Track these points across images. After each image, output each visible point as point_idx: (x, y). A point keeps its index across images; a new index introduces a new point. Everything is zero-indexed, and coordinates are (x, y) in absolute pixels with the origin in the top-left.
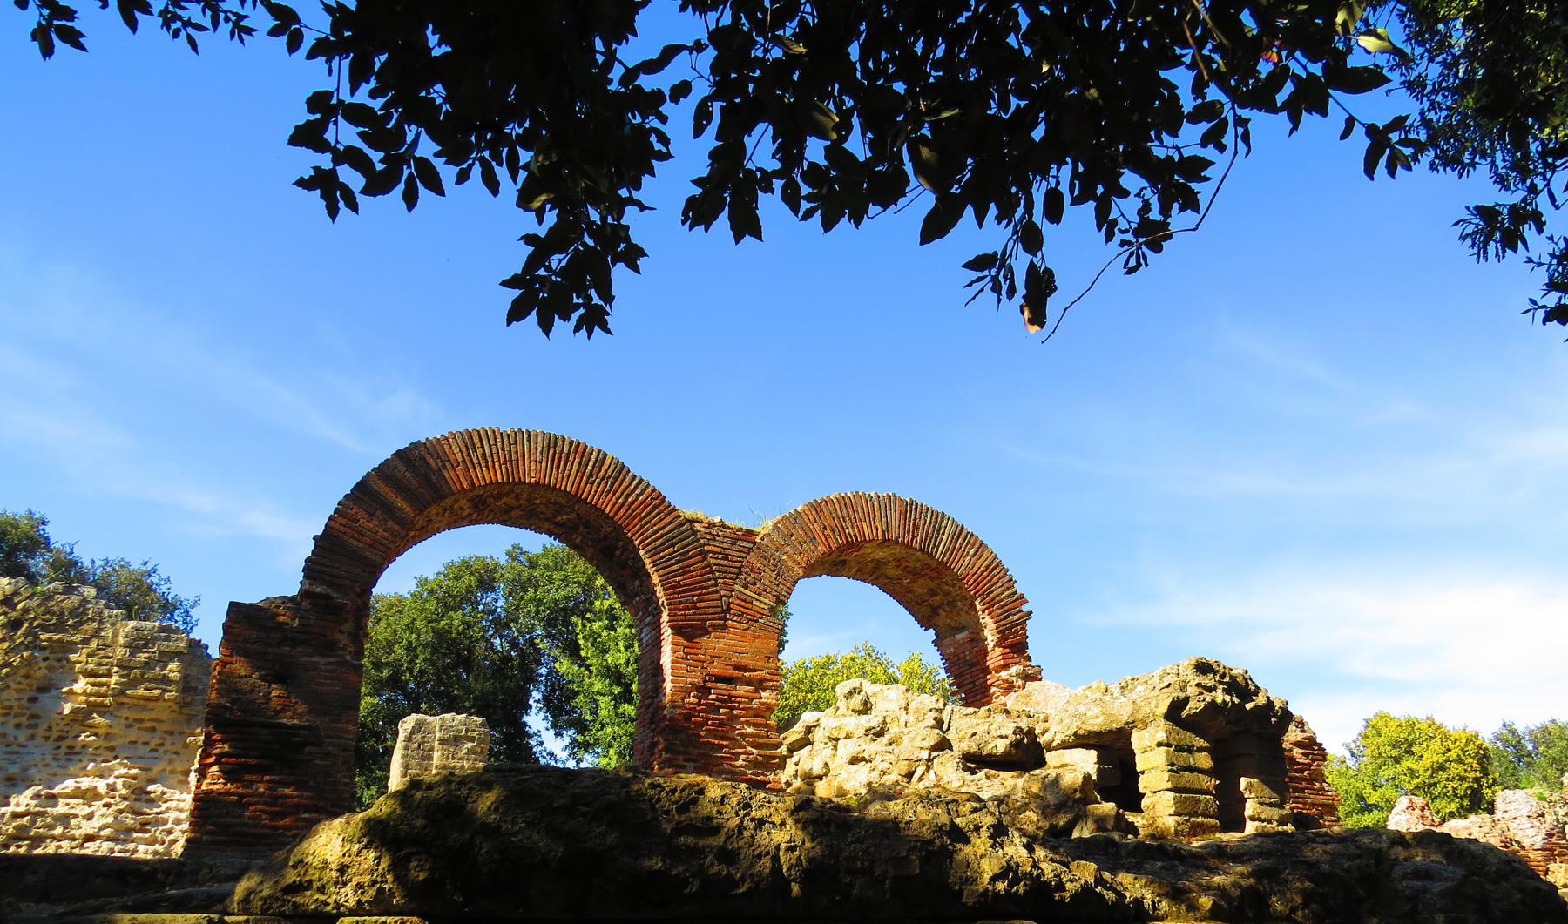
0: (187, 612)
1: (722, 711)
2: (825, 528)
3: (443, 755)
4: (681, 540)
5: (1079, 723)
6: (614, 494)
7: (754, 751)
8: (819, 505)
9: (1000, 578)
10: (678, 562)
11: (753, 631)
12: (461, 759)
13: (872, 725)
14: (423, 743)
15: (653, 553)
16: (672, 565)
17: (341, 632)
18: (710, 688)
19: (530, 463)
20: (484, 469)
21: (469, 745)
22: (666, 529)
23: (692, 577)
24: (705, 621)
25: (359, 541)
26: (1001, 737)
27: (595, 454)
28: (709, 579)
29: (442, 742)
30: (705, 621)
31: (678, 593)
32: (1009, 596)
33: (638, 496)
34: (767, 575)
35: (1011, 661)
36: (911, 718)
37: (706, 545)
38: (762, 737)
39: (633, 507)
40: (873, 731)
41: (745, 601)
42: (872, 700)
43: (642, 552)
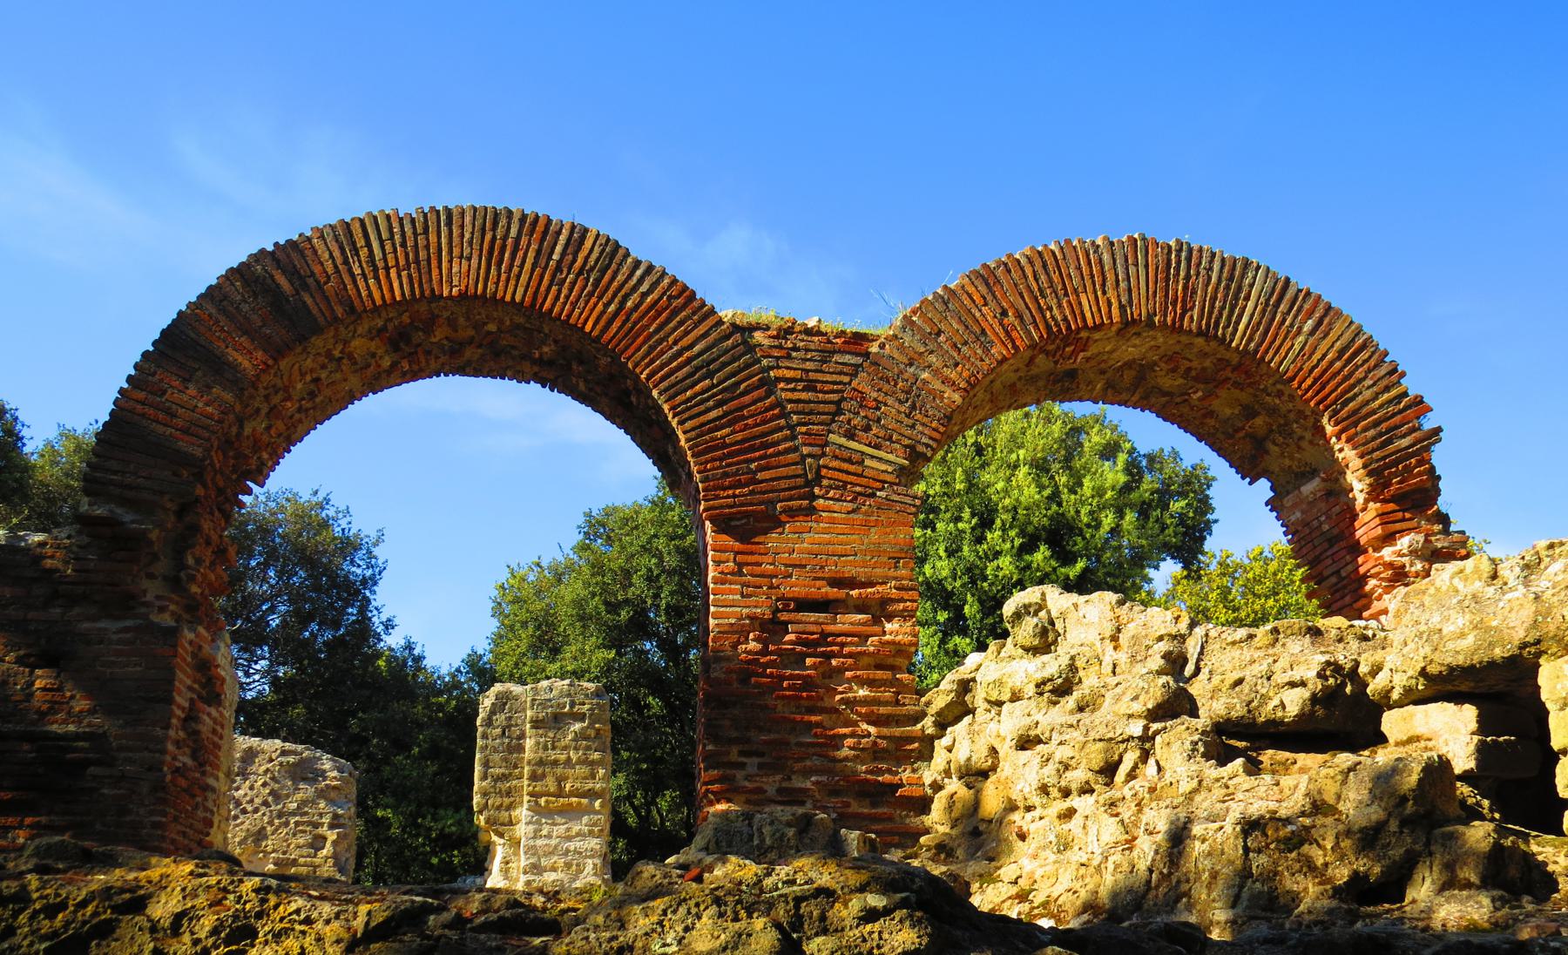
0: (369, 552)
1: (809, 661)
2: (1004, 313)
3: (538, 743)
4: (725, 365)
5: (1428, 649)
6: (600, 298)
7: (872, 729)
8: (992, 272)
9: (1370, 370)
10: (719, 404)
11: (866, 513)
12: (565, 748)
13: (1046, 674)
14: (509, 726)
15: (672, 393)
16: (709, 410)
17: (151, 576)
18: (786, 623)
19: (450, 261)
20: (371, 281)
21: (577, 726)
22: (697, 349)
23: (747, 427)
24: (773, 503)
25: (165, 425)
26: (1293, 685)
27: (565, 232)
28: (781, 429)
29: (537, 724)
30: (773, 503)
31: (721, 459)
32: (1389, 402)
33: (644, 295)
34: (893, 410)
35: (1398, 526)
36: (1122, 657)
37: (772, 368)
38: (886, 703)
39: (635, 316)
40: (1049, 687)
41: (849, 461)
42: (1059, 626)
43: (655, 393)
